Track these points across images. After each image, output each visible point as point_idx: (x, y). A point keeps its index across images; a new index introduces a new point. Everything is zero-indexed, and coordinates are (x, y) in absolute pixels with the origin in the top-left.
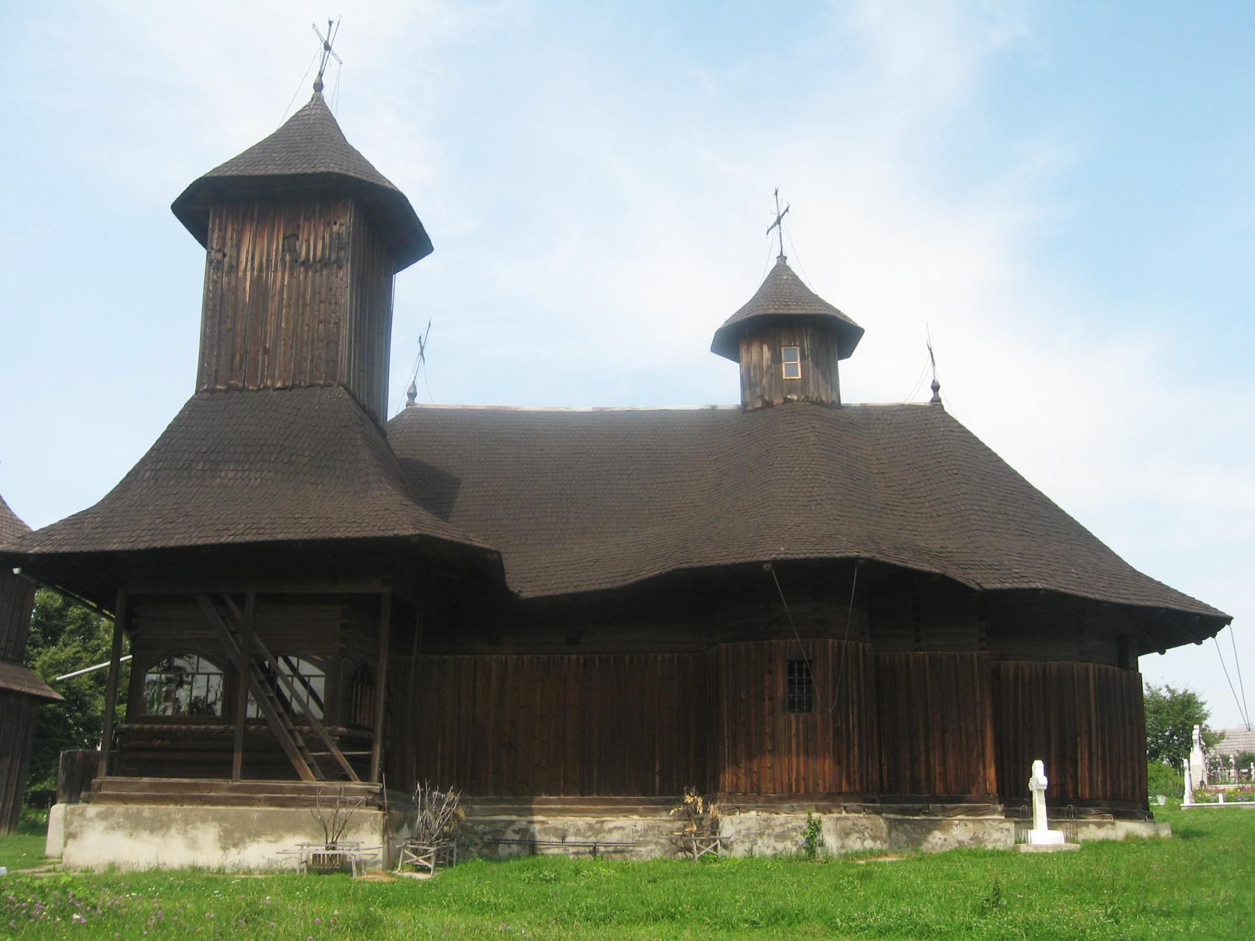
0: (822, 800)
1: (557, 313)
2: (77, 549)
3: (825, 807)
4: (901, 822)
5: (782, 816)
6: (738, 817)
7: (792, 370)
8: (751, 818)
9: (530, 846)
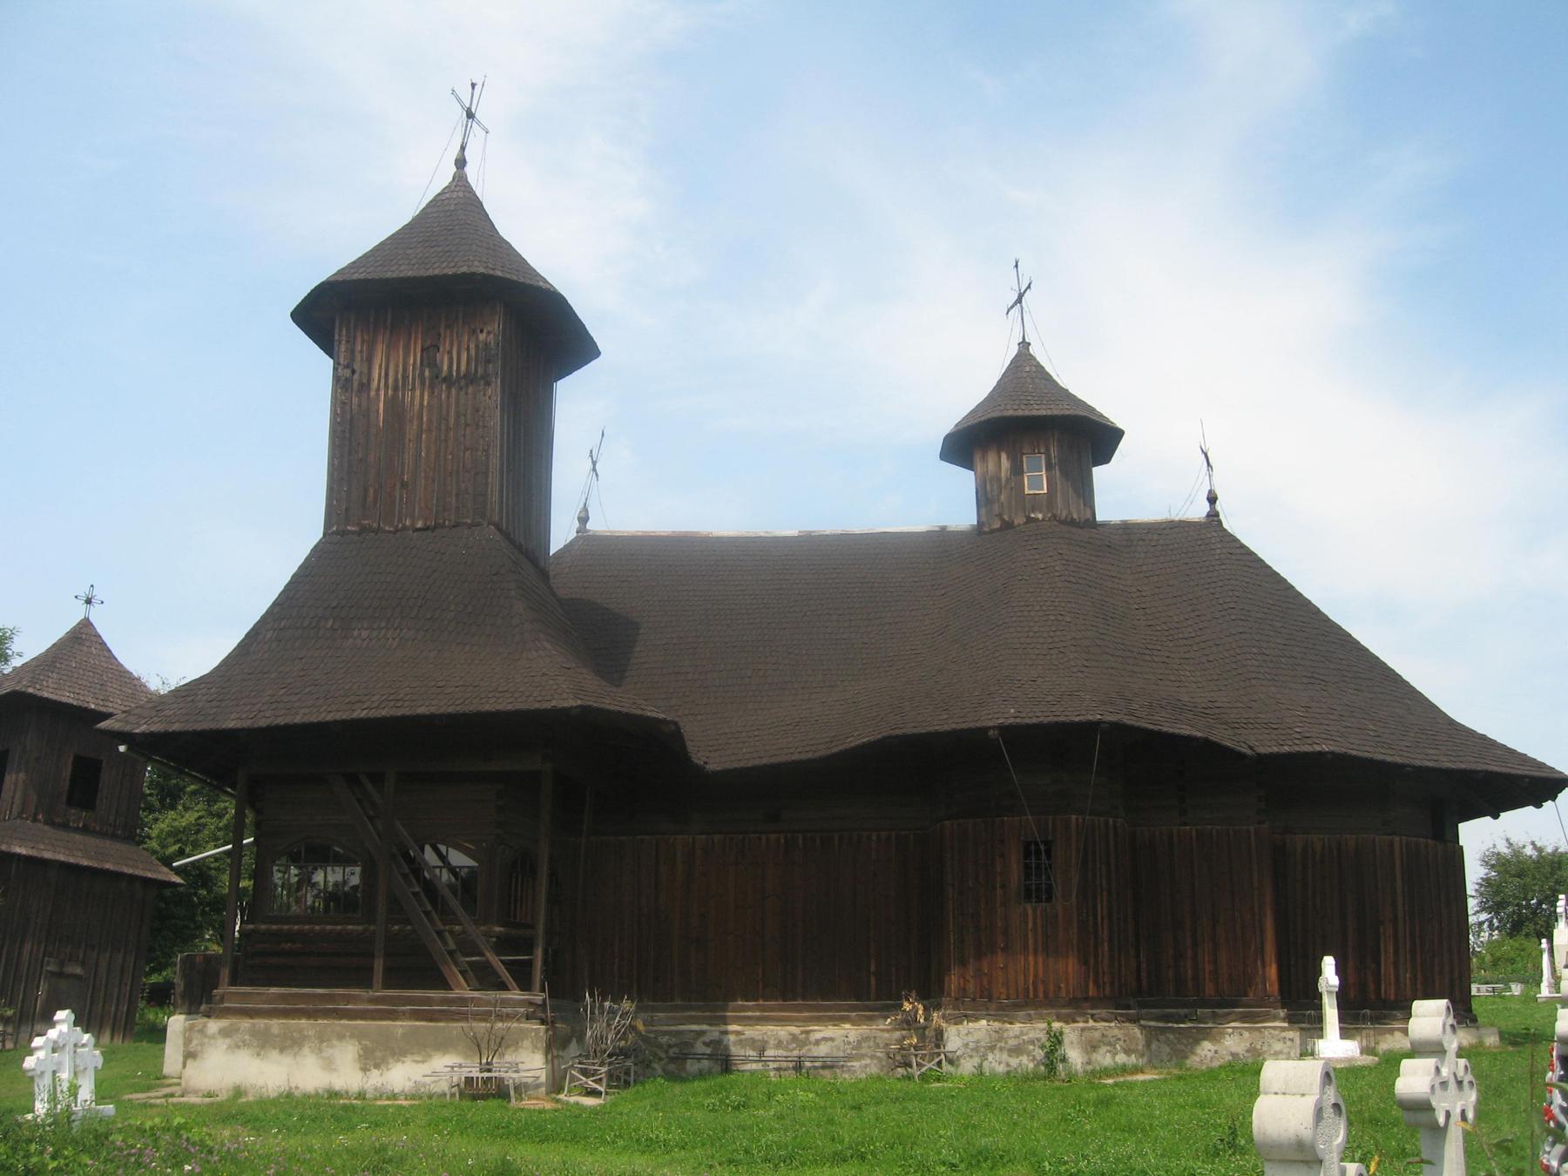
0: (1064, 1006)
1: (743, 421)
2: (190, 727)
3: (1068, 1015)
4: (1163, 1030)
5: (1018, 1026)
6: (967, 1026)
7: (1036, 483)
8: (981, 1028)
9: (725, 1063)
